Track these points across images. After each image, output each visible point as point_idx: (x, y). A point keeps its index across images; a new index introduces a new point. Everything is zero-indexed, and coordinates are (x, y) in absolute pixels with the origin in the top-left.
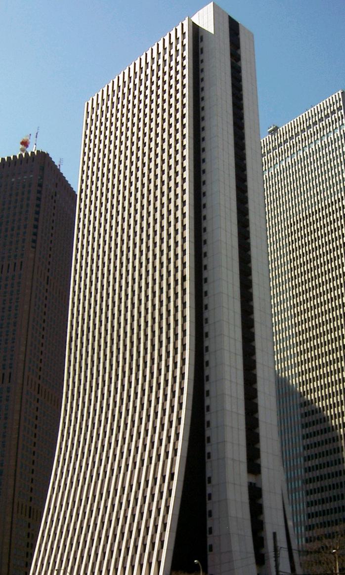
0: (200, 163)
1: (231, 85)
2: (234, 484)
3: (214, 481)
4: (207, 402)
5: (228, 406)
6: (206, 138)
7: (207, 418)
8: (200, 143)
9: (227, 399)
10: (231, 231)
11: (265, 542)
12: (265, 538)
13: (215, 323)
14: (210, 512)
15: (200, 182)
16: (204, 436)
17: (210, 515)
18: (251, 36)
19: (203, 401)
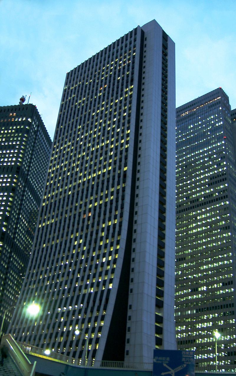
0: (137, 150)
1: (156, 273)
2: (147, 311)
3: (134, 308)
4: (132, 266)
5: (147, 260)
6: (145, 72)
7: (128, 325)
8: (127, 311)
9: (147, 255)
10: (157, 151)
11: (163, 342)
12: (163, 339)
13: (141, 224)
14: (129, 328)
15: (134, 195)
16: (127, 303)
17: (129, 330)
18: (174, 44)
19: (130, 255)
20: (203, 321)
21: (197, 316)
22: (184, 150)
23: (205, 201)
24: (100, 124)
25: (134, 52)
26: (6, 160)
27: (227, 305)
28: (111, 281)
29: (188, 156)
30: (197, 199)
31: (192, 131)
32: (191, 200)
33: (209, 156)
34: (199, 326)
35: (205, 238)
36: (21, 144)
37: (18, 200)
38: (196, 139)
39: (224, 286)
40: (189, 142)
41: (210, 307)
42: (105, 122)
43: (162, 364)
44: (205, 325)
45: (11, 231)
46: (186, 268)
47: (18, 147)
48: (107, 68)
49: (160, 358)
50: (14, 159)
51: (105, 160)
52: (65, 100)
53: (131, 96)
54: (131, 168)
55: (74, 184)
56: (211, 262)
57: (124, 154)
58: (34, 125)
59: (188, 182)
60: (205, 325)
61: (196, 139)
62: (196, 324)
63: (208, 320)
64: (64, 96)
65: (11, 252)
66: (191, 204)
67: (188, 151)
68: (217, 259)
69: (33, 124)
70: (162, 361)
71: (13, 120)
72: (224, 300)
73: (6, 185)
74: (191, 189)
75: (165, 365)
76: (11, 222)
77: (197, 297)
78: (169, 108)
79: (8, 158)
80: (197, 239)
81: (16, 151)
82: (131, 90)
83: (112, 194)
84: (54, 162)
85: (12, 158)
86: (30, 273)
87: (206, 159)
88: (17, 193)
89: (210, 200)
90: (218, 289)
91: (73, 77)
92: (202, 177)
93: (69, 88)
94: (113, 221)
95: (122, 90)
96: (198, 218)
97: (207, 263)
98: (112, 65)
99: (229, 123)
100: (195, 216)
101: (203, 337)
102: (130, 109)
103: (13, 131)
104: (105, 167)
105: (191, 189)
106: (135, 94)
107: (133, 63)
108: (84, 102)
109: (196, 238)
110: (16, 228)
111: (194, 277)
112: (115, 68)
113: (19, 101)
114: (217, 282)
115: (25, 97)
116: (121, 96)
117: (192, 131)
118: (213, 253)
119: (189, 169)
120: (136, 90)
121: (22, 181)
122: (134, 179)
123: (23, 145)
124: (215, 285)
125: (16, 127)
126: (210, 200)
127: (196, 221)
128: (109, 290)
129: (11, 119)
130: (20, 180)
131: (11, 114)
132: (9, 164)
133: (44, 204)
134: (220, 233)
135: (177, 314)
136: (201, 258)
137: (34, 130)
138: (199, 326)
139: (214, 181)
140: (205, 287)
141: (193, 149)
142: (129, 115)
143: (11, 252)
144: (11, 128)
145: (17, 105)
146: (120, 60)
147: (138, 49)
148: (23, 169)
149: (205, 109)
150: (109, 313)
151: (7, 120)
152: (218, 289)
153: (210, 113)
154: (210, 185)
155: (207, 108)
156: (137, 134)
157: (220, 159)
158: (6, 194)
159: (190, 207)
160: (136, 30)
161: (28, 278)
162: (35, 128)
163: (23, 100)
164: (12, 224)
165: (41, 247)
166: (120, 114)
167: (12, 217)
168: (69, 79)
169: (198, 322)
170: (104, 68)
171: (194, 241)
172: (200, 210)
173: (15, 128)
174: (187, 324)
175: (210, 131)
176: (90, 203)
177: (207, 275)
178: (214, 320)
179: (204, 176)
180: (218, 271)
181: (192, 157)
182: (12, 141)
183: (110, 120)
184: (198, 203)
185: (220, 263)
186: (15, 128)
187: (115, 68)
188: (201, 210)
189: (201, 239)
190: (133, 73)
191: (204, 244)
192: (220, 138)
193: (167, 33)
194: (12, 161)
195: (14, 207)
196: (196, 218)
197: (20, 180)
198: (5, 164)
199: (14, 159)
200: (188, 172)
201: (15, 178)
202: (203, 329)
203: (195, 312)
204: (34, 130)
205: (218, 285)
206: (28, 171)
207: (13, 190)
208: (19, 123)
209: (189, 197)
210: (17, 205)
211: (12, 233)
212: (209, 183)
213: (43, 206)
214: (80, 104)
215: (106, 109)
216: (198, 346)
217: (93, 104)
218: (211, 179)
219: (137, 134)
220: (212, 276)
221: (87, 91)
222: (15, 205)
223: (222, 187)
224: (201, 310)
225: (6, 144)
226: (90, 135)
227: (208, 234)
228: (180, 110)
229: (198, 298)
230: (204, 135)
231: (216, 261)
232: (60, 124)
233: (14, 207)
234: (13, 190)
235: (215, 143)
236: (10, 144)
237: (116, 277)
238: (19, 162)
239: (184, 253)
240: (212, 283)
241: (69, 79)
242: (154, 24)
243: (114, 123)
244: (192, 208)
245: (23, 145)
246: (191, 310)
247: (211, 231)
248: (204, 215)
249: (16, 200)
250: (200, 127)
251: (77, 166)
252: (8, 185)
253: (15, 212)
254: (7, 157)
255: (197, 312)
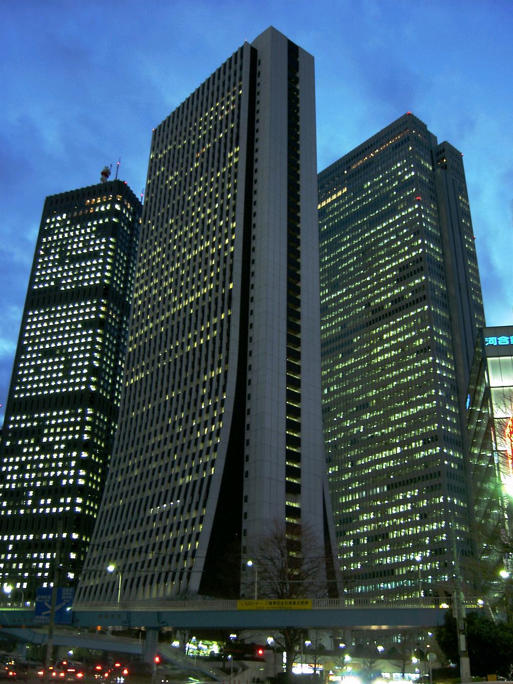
3: (250, 500)
18: (311, 59)
20: (398, 503)
21: (389, 495)
22: (360, 226)
23: (415, 299)
24: (198, 215)
25: (240, 88)
26: (87, 277)
27: (427, 476)
28: (213, 463)
29: (366, 235)
30: (380, 307)
31: (370, 192)
32: (373, 309)
33: (396, 232)
34: (393, 511)
35: (396, 368)
36: (108, 249)
37: (111, 339)
38: (375, 205)
39: (425, 445)
40: (365, 211)
41: (408, 481)
42: (204, 210)
43: (43, 603)
44: (402, 509)
45: (105, 389)
46: (371, 420)
47: (102, 254)
48: (206, 119)
49: (42, 597)
50: (99, 275)
51: (205, 273)
52: (153, 177)
53: (236, 165)
54: (239, 284)
55: (167, 314)
56: (406, 408)
57: (229, 261)
58: (125, 215)
59: (368, 279)
60: (402, 509)
61: (375, 205)
62: (419, 501)
63: (405, 501)
64: (150, 169)
65: (109, 422)
66: (374, 315)
67: (365, 227)
68: (414, 401)
69: (124, 212)
70: (43, 599)
71: (91, 211)
72: (426, 467)
73: (83, 318)
74: (371, 290)
75: (46, 604)
76: (103, 376)
77: (427, 455)
78: (302, 172)
79: (89, 273)
80: (384, 372)
81: (101, 261)
82: (237, 155)
83: (215, 326)
84: (142, 281)
85: (95, 272)
86: (116, 457)
87: (392, 238)
88: (109, 328)
89: (400, 305)
90: (418, 450)
91: (166, 133)
92: (387, 268)
93: (157, 156)
94: (217, 371)
95: (225, 156)
96: (385, 336)
97: (399, 410)
98: (211, 114)
99: (427, 170)
100: (380, 335)
101: (399, 528)
102: (235, 186)
103: (94, 229)
104: (205, 285)
105: (371, 290)
106: (241, 160)
107: (239, 108)
108: (176, 178)
109: (382, 370)
110: (115, 382)
111: (382, 434)
112: (216, 118)
113: (100, 176)
114: (416, 439)
115: (109, 168)
116: (224, 165)
117: (370, 192)
118: (406, 393)
119: (367, 258)
120: (243, 155)
121: (115, 308)
122: (246, 299)
123: (111, 250)
124: (413, 444)
125: (98, 222)
126: (400, 305)
127: (382, 342)
128: (210, 477)
129: (89, 210)
130: (112, 306)
131: (88, 201)
132: (92, 283)
133: (131, 349)
134: (418, 360)
135: (375, 490)
136: (391, 401)
137: (126, 221)
138: (393, 511)
139: (405, 273)
140: (399, 448)
141: (373, 223)
142: (234, 197)
143: (109, 422)
144: (89, 224)
145: (96, 184)
146: (222, 104)
147: (246, 82)
148: (115, 289)
149: (388, 152)
150: (209, 512)
151: (83, 212)
152: (418, 450)
153: (395, 159)
154: (400, 280)
155: (391, 150)
156: (248, 226)
157: (412, 236)
158: (91, 332)
159: (371, 320)
160: (242, 49)
161: (114, 466)
162: (128, 218)
163: (106, 174)
164: (106, 378)
165: (130, 417)
166: (222, 197)
167: (104, 367)
168: (156, 141)
169: (391, 505)
170: (218, 104)
171: (380, 375)
172: (386, 324)
173: (95, 223)
174: (375, 509)
175: (396, 188)
176: (188, 344)
177: (401, 428)
178: (414, 500)
179: (389, 267)
180: (415, 421)
181: (372, 235)
182: (94, 246)
183: (210, 206)
184: (383, 313)
185: (419, 407)
186: (95, 223)
187: (216, 118)
188: (388, 323)
189: (390, 371)
190: (238, 126)
191: (396, 378)
192: (410, 202)
193: (297, 41)
194: (96, 278)
195: (106, 350)
196: (381, 339)
197: (112, 306)
198: (86, 284)
199: (99, 275)
200: (367, 261)
201: (103, 305)
202: (398, 515)
203: (386, 489)
204: (126, 221)
205: (417, 444)
206: (125, 288)
207: (101, 324)
208: (101, 215)
209: (369, 304)
210: (110, 347)
211: (108, 393)
212: (399, 277)
213: (130, 353)
214: (171, 182)
215: (205, 190)
216: (393, 542)
217: (187, 182)
218: (400, 271)
219: (248, 226)
220: (408, 430)
221: (181, 161)
222: (107, 347)
223: (417, 281)
224: (395, 487)
225: (85, 251)
226: (186, 234)
227: (398, 362)
228: (367, 146)
229: (390, 467)
230: (386, 198)
231: (413, 405)
232: (147, 218)
233: (106, 350)
234: (101, 324)
235: (405, 208)
236: (91, 250)
237: (220, 457)
238: (107, 278)
239: (366, 397)
240: (409, 442)
241: (156, 141)
242: (273, 33)
243: (215, 211)
244: (372, 323)
245: (111, 250)
246: (381, 486)
247: (404, 357)
248: (393, 333)
249: (108, 339)
250: (381, 185)
251: (171, 285)
252: (93, 317)
253: (108, 358)
254: (87, 273)
255: (388, 488)
